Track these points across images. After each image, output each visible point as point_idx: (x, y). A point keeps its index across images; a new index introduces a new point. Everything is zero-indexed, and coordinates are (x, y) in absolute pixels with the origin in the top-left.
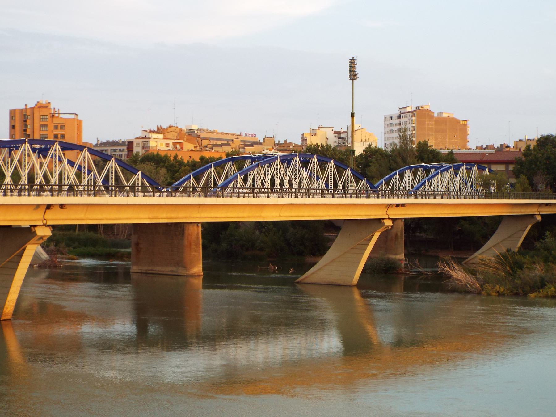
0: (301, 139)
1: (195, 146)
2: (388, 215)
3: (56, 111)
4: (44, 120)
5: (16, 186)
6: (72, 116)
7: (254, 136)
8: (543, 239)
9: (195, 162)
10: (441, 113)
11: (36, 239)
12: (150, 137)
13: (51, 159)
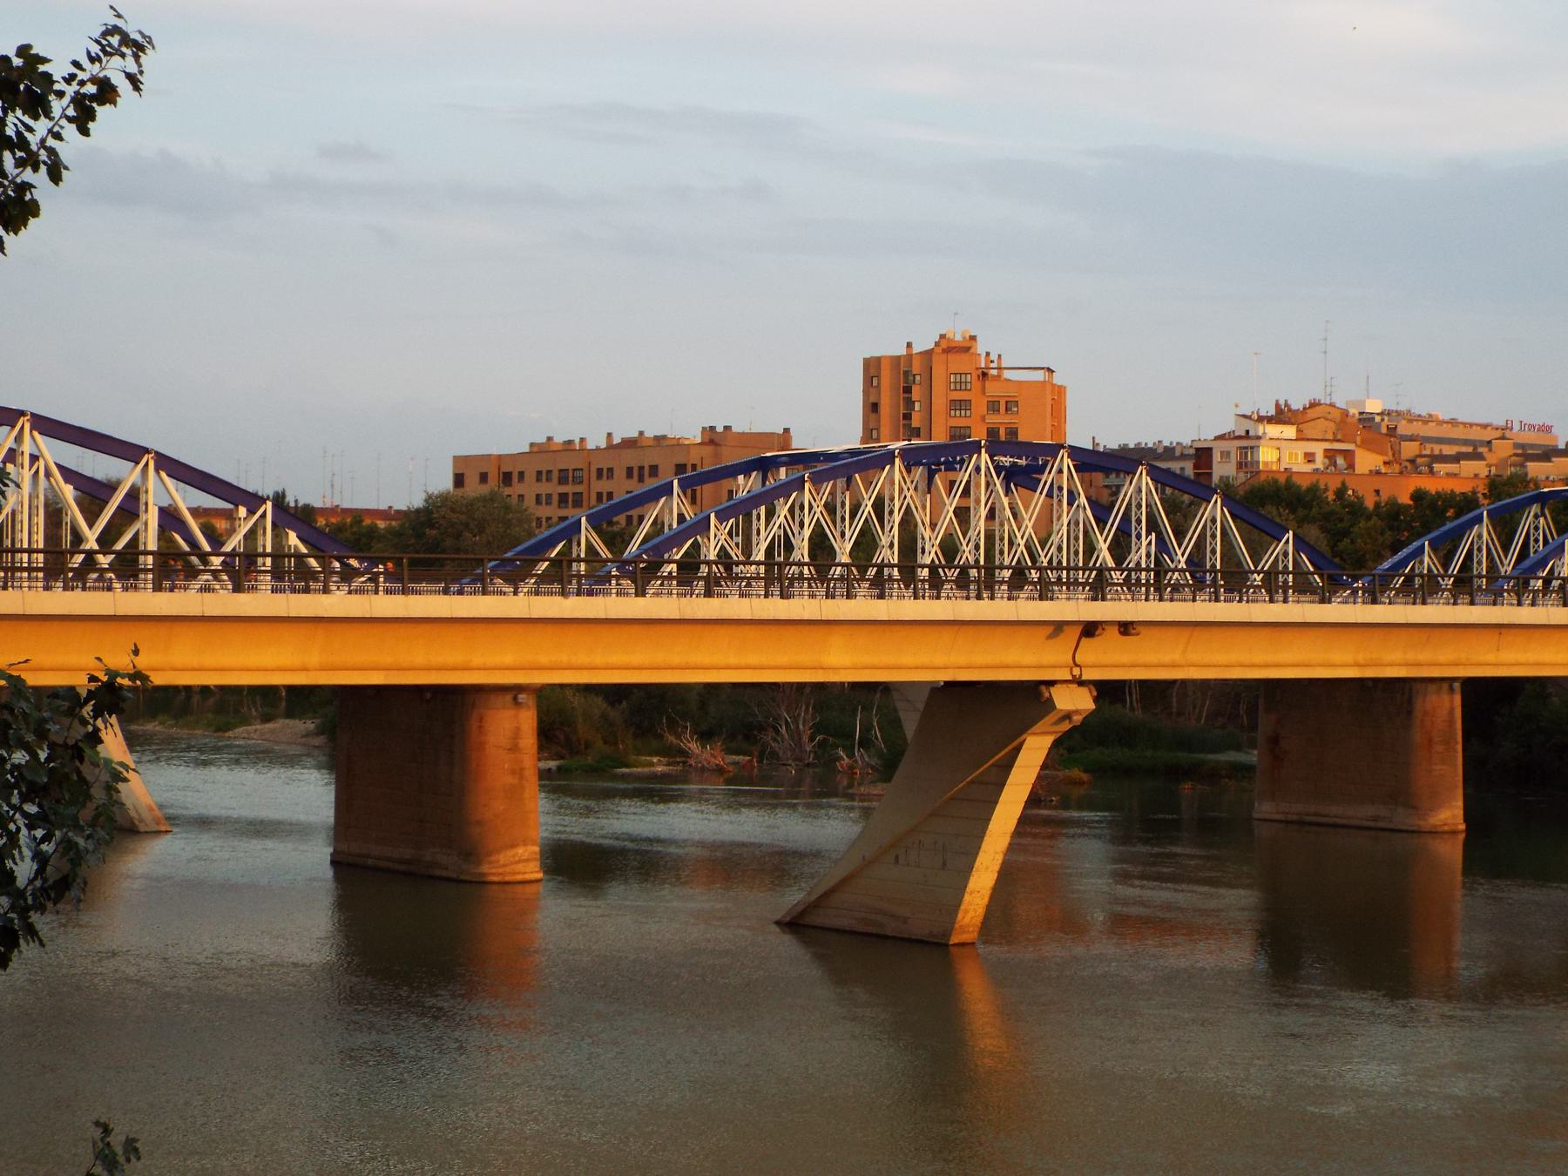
1: (1386, 459)
3: (992, 362)
5: (863, 570)
6: (1039, 376)
7: (1547, 429)
9: (1399, 505)
11: (1053, 720)
12: (1260, 433)
13: (1048, 499)
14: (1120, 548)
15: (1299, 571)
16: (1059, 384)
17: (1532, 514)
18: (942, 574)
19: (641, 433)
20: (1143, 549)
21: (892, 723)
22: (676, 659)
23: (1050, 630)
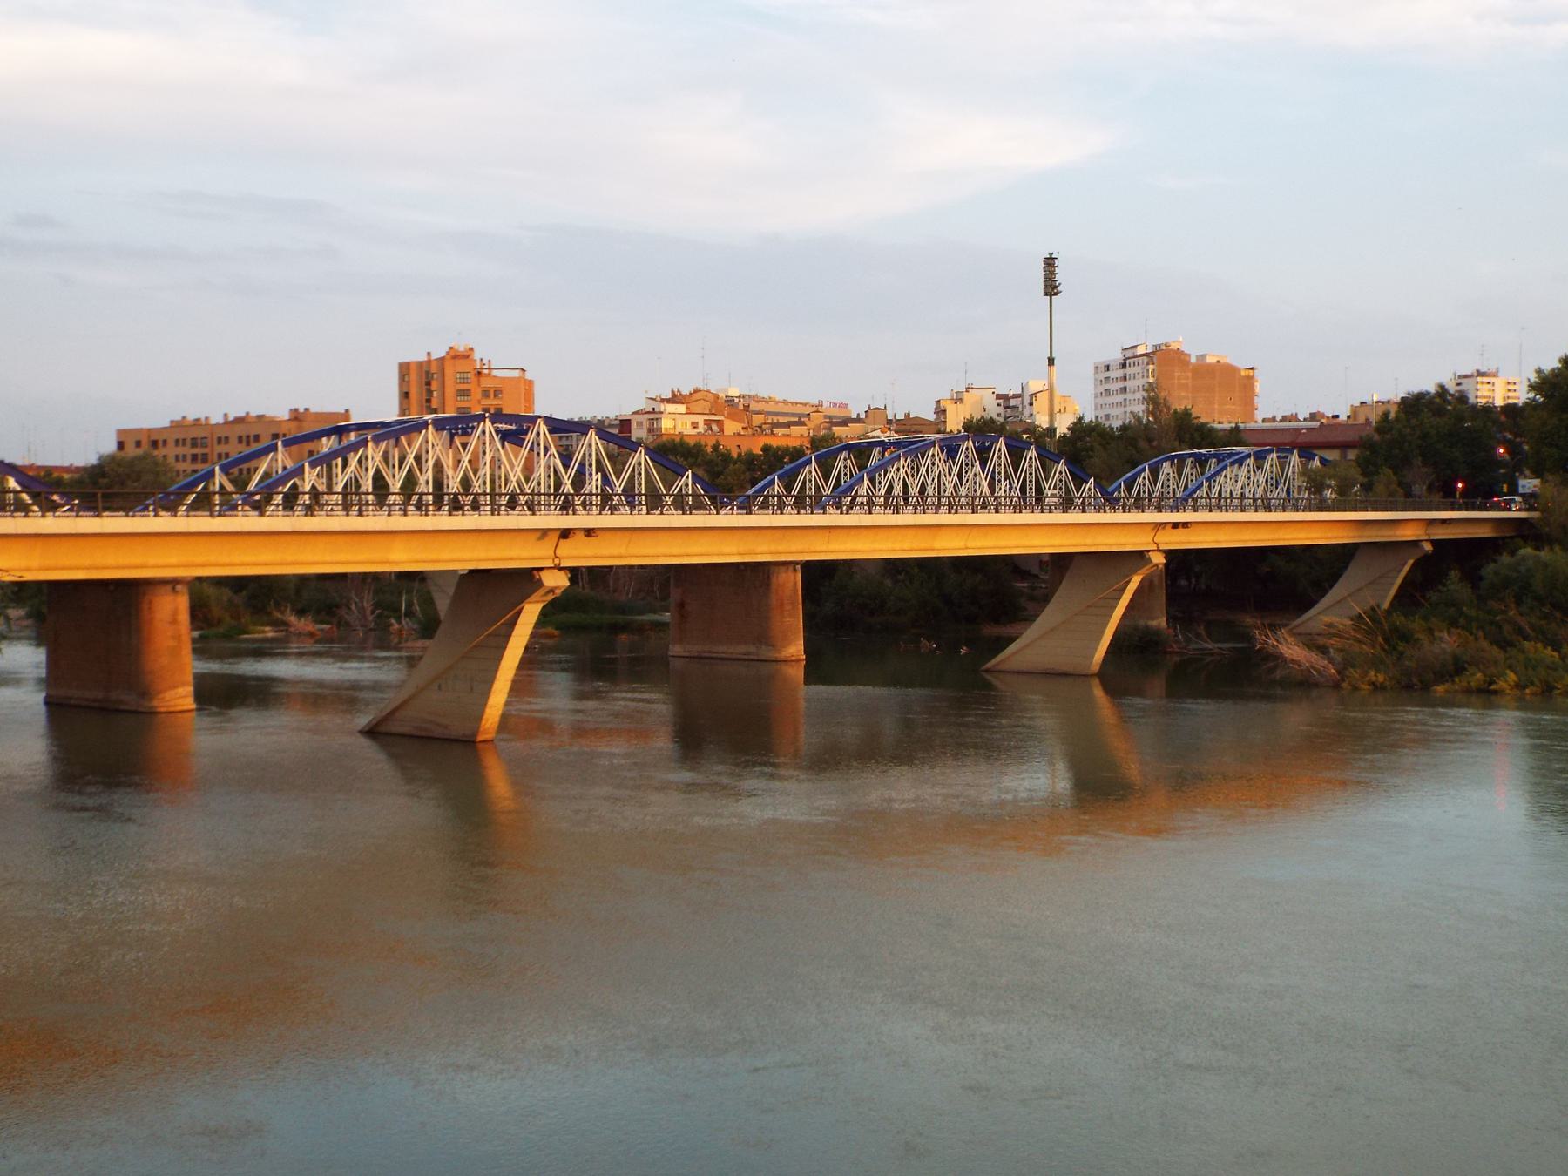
0: (933, 411)
2: (1158, 544)
4: (464, 380)
5: (409, 498)
6: (516, 374)
8: (1444, 585)
10: (1204, 356)
12: (662, 410)
14: (579, 482)
15: (696, 495)
16: (529, 379)
17: (842, 458)
18: (461, 499)
19: (248, 413)
20: (594, 483)
21: (428, 601)
22: (290, 558)
23: (538, 534)
